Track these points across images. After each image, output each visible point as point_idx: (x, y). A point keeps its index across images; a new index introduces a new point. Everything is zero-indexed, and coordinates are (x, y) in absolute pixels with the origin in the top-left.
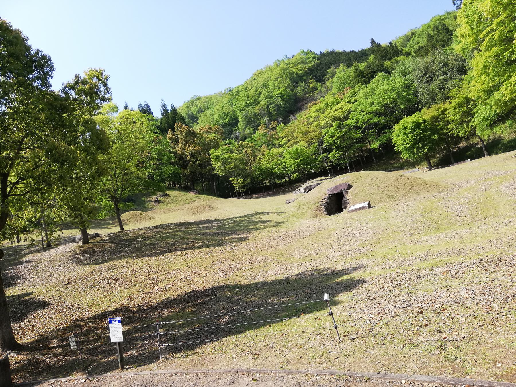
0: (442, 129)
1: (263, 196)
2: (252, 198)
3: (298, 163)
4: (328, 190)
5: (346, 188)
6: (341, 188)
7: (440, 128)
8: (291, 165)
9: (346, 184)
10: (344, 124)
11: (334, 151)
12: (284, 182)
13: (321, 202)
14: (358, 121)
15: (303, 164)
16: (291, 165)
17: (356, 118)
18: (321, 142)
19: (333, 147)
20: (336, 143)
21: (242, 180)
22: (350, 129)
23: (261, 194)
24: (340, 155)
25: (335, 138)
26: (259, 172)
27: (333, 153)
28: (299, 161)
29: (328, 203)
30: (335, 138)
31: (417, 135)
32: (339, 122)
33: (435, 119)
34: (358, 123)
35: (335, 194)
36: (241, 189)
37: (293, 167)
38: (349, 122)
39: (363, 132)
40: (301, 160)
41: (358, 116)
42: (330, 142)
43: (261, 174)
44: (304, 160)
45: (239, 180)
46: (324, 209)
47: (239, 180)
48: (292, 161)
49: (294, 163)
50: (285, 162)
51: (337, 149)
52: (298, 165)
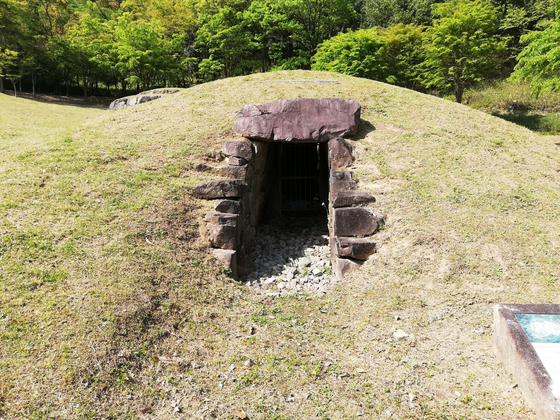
0: (403, 67)
1: (60, 101)
2: (39, 99)
3: (142, 56)
4: (244, 114)
5: (345, 126)
6: (321, 120)
7: (400, 66)
8: (129, 58)
9: (345, 107)
10: (238, 18)
11: (210, 58)
12: (112, 90)
13: (201, 168)
14: (263, 17)
15: (152, 63)
16: (129, 58)
17: (259, 10)
18: (191, 38)
19: (210, 50)
20: (217, 45)
21: (15, 53)
22: (245, 28)
23: (60, 98)
24: (219, 68)
25: (217, 36)
26: (59, 52)
27: (208, 60)
28: (144, 53)
29: (241, 190)
30: (217, 36)
31: (367, 64)
32: (230, 9)
33: (396, 47)
34: (261, 20)
35: (282, 143)
36: (10, 73)
37: (131, 61)
38: (246, 14)
39: (265, 40)
40: (150, 54)
41: (263, 9)
42: (208, 39)
43: (64, 58)
44: (155, 55)
45: (8, 51)
46: (216, 230)
47: (8, 51)
48: (131, 51)
49: (135, 56)
50: (117, 48)
51: (218, 56)
52: (142, 60)
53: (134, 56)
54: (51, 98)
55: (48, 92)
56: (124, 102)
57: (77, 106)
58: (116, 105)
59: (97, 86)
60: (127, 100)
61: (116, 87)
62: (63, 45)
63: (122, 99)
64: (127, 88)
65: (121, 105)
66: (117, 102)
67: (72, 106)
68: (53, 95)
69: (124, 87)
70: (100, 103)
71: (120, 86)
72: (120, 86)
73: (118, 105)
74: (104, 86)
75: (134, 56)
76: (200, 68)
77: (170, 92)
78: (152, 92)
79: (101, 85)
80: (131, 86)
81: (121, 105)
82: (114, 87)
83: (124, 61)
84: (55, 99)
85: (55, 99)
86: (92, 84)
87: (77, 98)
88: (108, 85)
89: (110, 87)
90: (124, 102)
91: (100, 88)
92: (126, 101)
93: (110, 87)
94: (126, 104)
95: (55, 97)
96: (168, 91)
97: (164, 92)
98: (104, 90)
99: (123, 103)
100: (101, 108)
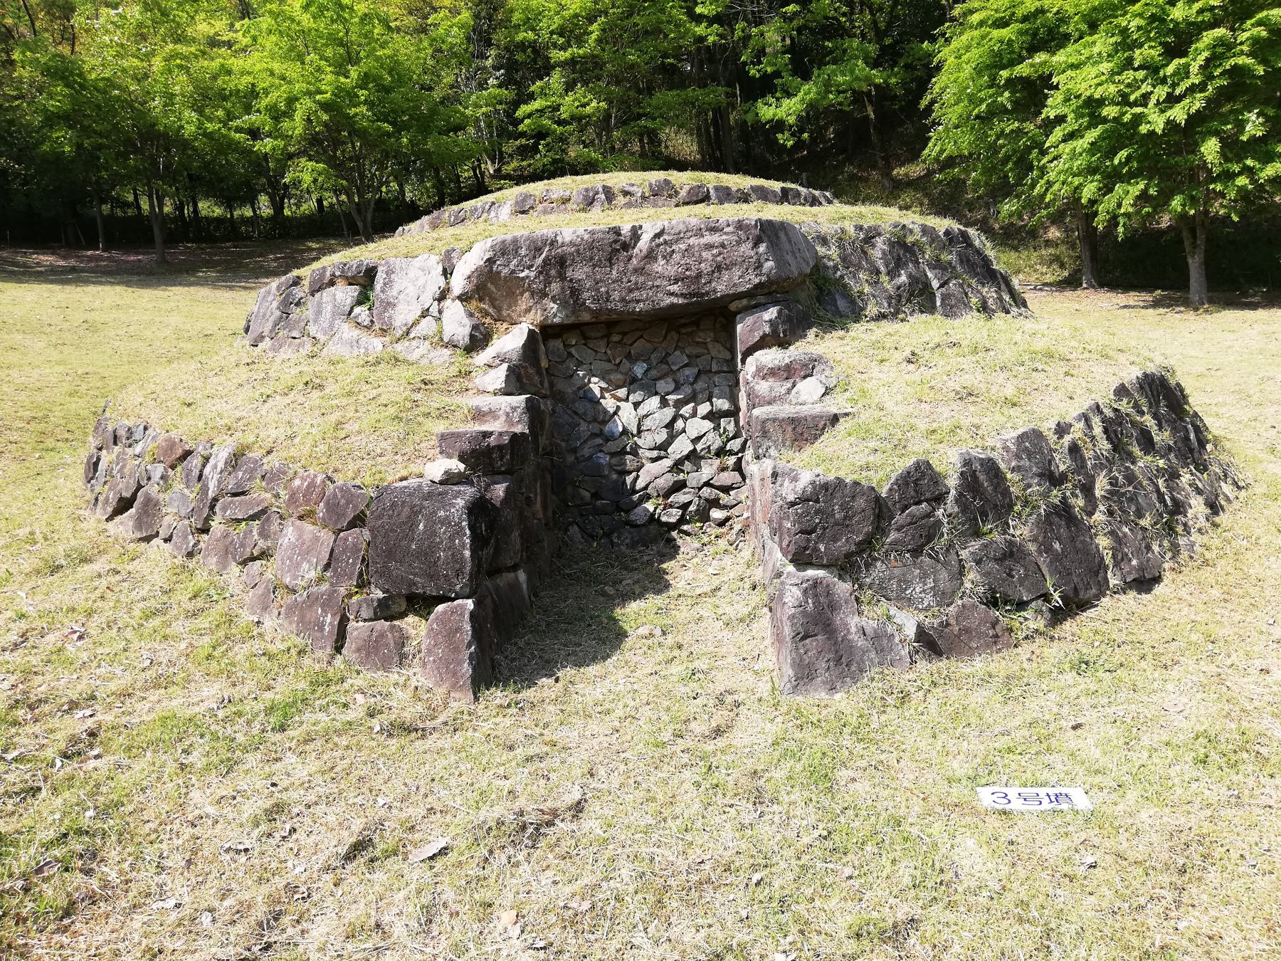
12: (244, 220)
51: (581, 72)
53: (309, 93)
54: (47, 259)
55: (43, 241)
56: (354, 291)
57: (128, 284)
58: (296, 312)
59: (196, 211)
60: (371, 273)
61: (254, 211)
62: (64, 72)
63: (331, 262)
64: (287, 212)
65: (328, 310)
66: (298, 292)
67: (107, 288)
68: (60, 248)
69: (278, 207)
70: (210, 265)
71: (265, 207)
72: (265, 207)
73: (309, 312)
74: (218, 211)
75: (309, 93)
76: (522, 121)
77: (621, 200)
78: (505, 211)
79: (209, 208)
80: (298, 205)
81: (328, 310)
82: (248, 212)
83: (277, 115)
84: (62, 263)
85: (62, 263)
86: (180, 208)
87: (137, 254)
88: (231, 208)
89: (237, 213)
90: (354, 291)
91: (206, 218)
92: (365, 279)
93: (237, 213)
94: (362, 299)
95: (64, 258)
96: (609, 194)
97: (589, 202)
98: (219, 221)
99: (344, 294)
100: (213, 284)
